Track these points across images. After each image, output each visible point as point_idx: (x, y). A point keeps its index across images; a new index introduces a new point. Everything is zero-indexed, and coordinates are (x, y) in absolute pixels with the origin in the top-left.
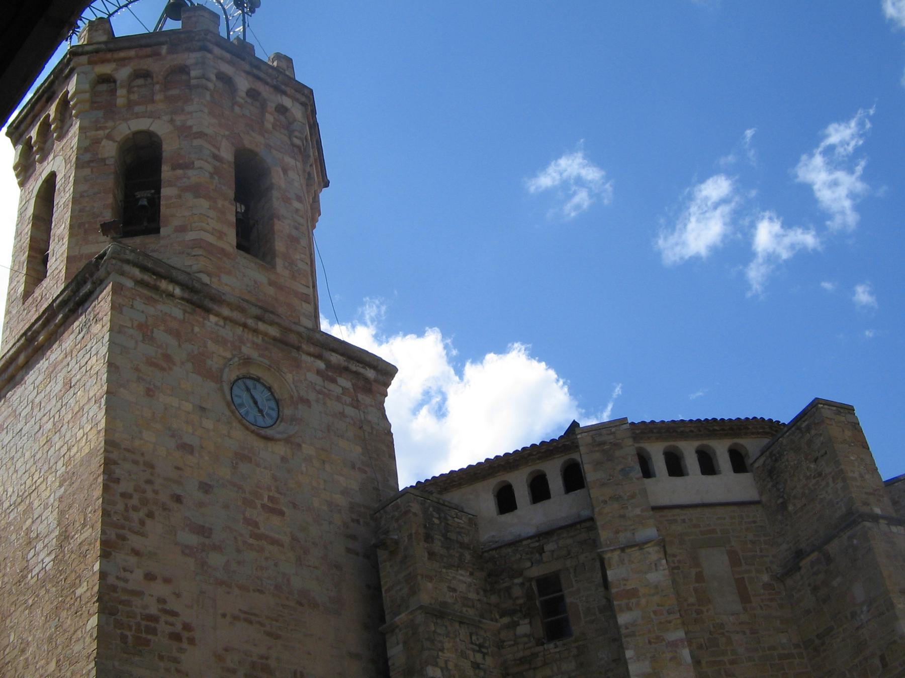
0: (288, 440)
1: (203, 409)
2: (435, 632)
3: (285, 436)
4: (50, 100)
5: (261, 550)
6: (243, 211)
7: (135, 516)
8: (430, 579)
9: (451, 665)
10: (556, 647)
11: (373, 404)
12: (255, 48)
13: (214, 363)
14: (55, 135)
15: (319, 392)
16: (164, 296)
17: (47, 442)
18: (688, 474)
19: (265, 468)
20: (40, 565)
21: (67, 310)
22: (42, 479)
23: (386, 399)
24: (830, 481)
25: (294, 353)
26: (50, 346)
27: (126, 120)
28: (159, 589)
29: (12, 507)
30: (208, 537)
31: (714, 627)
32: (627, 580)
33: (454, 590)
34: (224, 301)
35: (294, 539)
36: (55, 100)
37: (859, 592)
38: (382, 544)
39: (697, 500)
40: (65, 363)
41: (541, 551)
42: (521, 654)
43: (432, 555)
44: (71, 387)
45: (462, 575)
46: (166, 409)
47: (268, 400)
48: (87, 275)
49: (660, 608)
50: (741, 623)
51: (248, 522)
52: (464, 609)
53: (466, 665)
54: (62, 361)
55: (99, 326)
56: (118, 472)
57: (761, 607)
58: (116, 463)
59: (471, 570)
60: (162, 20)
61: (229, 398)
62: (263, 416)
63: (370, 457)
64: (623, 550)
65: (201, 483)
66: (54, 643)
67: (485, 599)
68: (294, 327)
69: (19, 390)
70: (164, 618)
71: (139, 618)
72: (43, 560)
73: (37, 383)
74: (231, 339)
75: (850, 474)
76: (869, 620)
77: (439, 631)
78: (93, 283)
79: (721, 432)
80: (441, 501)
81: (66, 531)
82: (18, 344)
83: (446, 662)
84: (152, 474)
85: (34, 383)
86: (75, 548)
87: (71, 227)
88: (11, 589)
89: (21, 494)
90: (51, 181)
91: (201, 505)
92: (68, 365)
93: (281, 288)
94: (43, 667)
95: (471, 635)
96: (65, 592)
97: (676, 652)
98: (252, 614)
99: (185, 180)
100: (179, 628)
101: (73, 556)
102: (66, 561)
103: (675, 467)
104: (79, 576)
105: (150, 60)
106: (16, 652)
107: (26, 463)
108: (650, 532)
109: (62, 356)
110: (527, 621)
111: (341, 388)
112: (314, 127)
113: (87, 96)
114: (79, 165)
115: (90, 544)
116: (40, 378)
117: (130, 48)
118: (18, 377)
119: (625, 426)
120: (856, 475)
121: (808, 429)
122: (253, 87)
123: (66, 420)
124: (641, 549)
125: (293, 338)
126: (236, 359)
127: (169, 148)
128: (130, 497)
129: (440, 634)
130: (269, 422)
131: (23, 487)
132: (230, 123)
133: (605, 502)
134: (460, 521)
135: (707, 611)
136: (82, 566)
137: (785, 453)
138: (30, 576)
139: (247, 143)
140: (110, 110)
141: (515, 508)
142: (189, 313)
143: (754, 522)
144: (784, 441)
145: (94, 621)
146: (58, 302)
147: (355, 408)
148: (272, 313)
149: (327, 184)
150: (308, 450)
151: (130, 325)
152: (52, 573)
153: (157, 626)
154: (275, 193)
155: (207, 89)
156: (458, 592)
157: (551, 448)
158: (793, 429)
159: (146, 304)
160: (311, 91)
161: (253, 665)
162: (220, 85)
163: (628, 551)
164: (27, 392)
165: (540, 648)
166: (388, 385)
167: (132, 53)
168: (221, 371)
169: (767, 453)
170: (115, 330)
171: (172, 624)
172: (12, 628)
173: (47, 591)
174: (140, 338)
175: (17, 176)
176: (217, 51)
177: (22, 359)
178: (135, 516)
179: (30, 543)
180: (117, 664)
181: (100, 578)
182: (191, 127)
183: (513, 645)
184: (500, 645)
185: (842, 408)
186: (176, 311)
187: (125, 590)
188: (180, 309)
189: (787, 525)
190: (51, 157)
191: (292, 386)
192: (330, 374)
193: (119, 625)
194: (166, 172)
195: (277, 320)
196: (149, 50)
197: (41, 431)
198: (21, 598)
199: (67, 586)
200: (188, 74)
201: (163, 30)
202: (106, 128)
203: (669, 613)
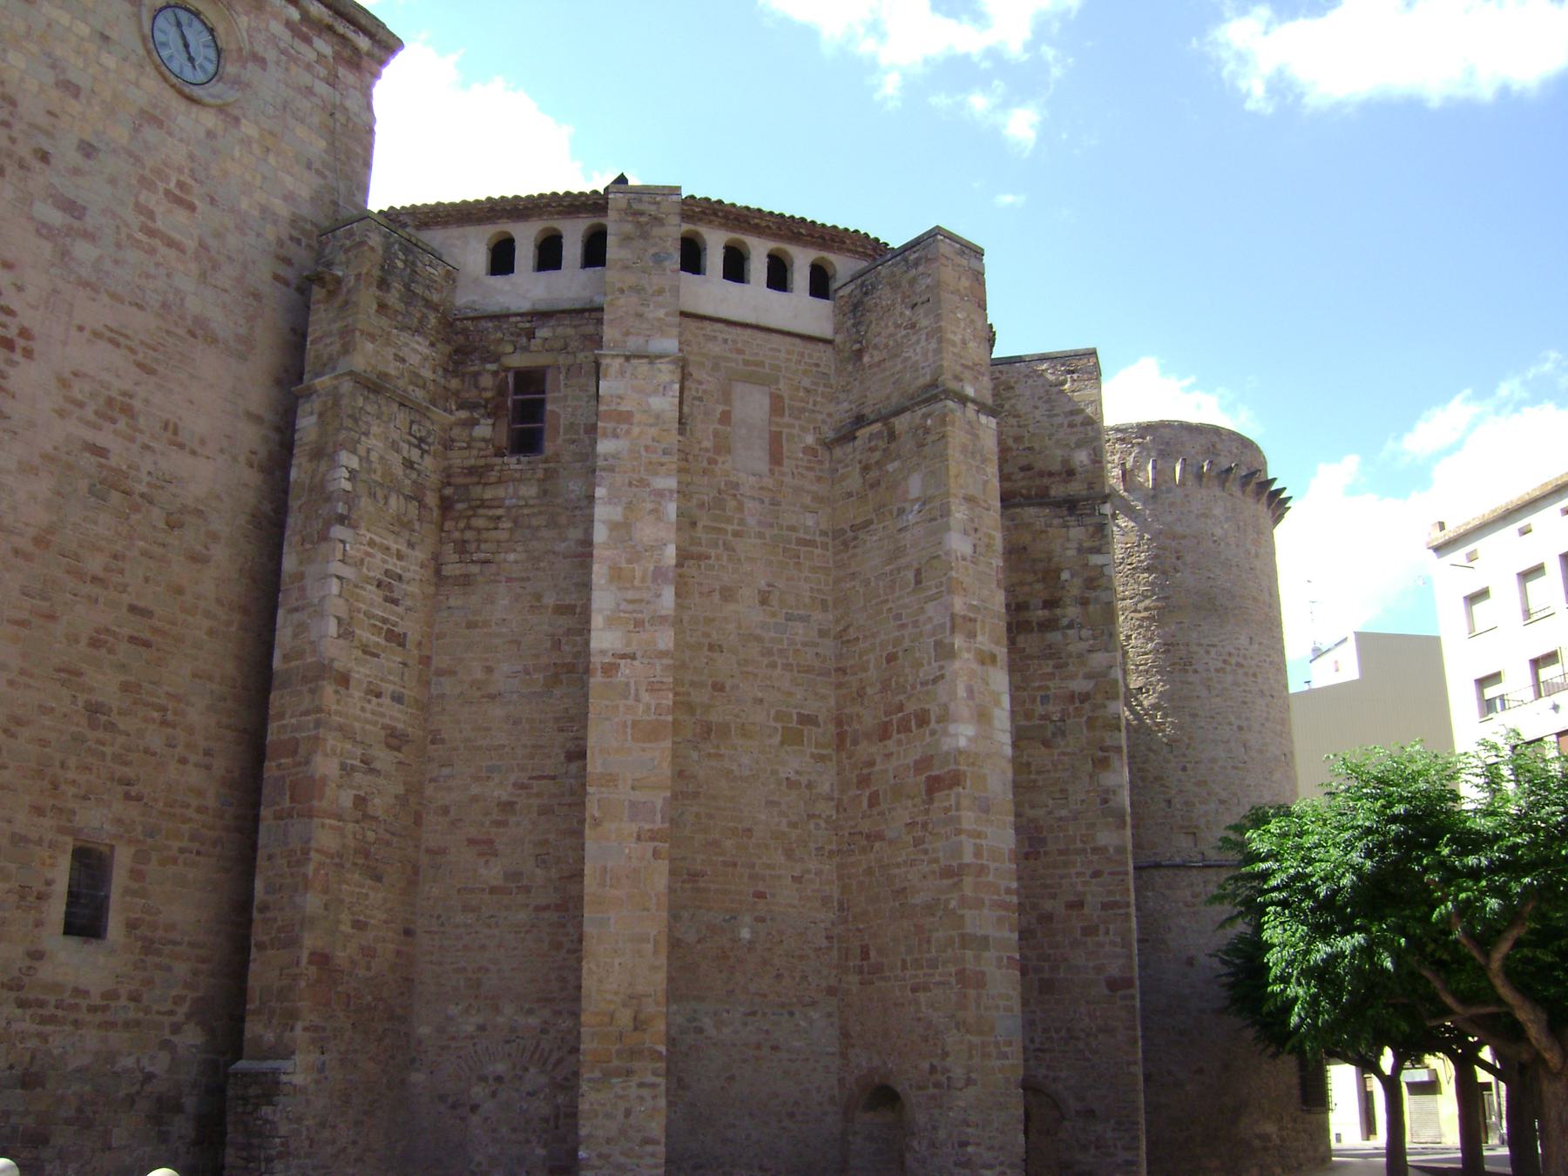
0: (221, 109)
1: (105, 38)
2: (362, 408)
3: (219, 102)
5: (152, 251)
8: (372, 337)
9: (374, 456)
10: (519, 462)
11: (359, 86)
15: (283, 52)
19: (181, 140)
24: (923, 337)
30: (79, 218)
31: (726, 484)
32: (621, 398)
33: (403, 360)
35: (203, 246)
37: (915, 486)
38: (317, 279)
41: (531, 335)
42: (472, 462)
43: (382, 307)
45: (418, 343)
46: (49, 25)
49: (656, 444)
50: (761, 488)
51: (141, 209)
52: (411, 388)
53: (395, 460)
61: (147, 30)
62: (194, 67)
64: (628, 358)
65: (82, 141)
67: (443, 381)
75: (950, 336)
76: (917, 523)
77: (369, 408)
80: (413, 240)
83: (369, 451)
84: (11, 114)
91: (76, 171)
95: (412, 422)
97: (660, 503)
103: (735, 267)
110: (490, 421)
119: (675, 198)
120: (957, 339)
121: (916, 264)
129: (369, 413)
130: (201, 77)
133: (622, 291)
134: (433, 271)
135: (723, 463)
144: (883, 270)
150: (248, 129)
158: (898, 258)
161: (110, 402)
163: (635, 362)
165: (498, 460)
166: (383, 63)
169: (859, 281)
183: (465, 449)
184: (448, 444)
185: (967, 247)
189: (855, 380)
191: (245, 34)
192: (304, 29)
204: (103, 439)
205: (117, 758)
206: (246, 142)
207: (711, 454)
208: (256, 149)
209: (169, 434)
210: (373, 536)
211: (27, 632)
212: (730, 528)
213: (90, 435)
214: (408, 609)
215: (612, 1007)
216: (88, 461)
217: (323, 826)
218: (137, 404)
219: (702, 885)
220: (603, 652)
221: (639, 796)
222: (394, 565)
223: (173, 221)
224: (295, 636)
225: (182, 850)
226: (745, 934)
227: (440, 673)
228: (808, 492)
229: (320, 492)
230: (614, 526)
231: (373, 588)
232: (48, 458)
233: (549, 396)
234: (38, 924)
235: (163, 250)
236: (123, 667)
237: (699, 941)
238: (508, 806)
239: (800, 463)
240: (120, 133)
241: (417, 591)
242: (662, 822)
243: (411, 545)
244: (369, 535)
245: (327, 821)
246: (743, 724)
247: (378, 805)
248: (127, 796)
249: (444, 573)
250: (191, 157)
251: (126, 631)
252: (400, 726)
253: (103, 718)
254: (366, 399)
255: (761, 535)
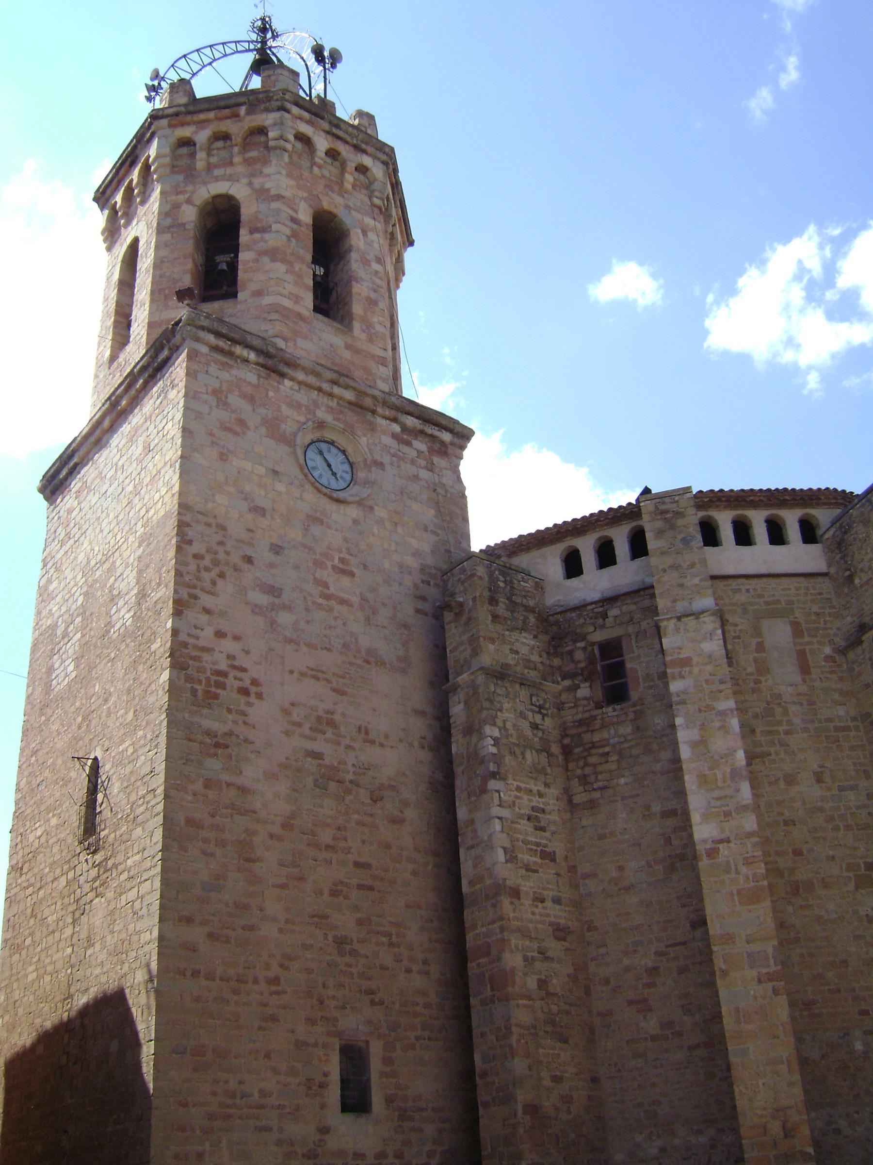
0: (359, 503)
1: (276, 473)
2: (494, 692)
3: (357, 499)
4: (133, 164)
5: (330, 610)
6: (322, 274)
7: (206, 576)
8: (492, 640)
9: (509, 725)
10: (614, 710)
12: (336, 106)
13: (288, 428)
14: (138, 200)
16: (239, 361)
17: (129, 503)
18: (755, 544)
19: (337, 530)
20: (121, 621)
21: (147, 375)
22: (123, 539)
23: (462, 462)
25: (369, 416)
26: (132, 411)
27: (205, 183)
28: (228, 645)
29: (98, 565)
30: (278, 597)
32: (680, 649)
33: (517, 652)
34: (299, 365)
35: (364, 599)
36: (138, 164)
38: (446, 606)
39: (763, 570)
40: (145, 428)
41: (605, 616)
42: (580, 716)
43: (495, 617)
44: (150, 451)
46: (239, 472)
47: (342, 463)
48: (164, 342)
50: (799, 694)
51: (318, 582)
52: (526, 671)
53: (525, 725)
54: (142, 425)
55: (175, 392)
56: (191, 533)
57: (820, 678)
58: (188, 525)
59: (535, 633)
60: (248, 77)
61: (302, 461)
63: (443, 520)
64: (679, 618)
65: (272, 544)
66: (132, 694)
67: (548, 662)
68: (370, 391)
69: (105, 453)
70: (233, 673)
71: (208, 674)
72: (123, 616)
73: (121, 446)
74: (306, 403)
77: (499, 691)
78: (170, 349)
79: (792, 502)
80: (508, 565)
81: (143, 590)
82: (104, 408)
83: (504, 722)
85: (117, 446)
86: (150, 607)
87: (153, 292)
88: (96, 643)
89: (105, 553)
90: (134, 245)
91: (272, 565)
92: (148, 429)
93: (357, 351)
94: (122, 716)
95: (531, 696)
96: (142, 647)
97: (725, 720)
98: (319, 671)
99: (262, 244)
100: (247, 683)
101: (150, 614)
102: (143, 618)
104: (154, 633)
105: (229, 121)
106: (100, 701)
107: (110, 523)
108: (708, 602)
109: (142, 420)
110: (587, 684)
111: (416, 452)
112: (396, 186)
113: (167, 160)
114: (161, 230)
115: (164, 603)
116: (123, 442)
117: (208, 110)
118: (104, 440)
122: (333, 146)
123: (145, 483)
124: (697, 618)
125: (368, 402)
126: (310, 423)
127: (247, 212)
128: (202, 557)
130: (343, 485)
131: (107, 546)
132: (309, 184)
133: (664, 571)
135: (766, 681)
136: (157, 623)
137: (855, 525)
138: (112, 631)
139: (326, 205)
140: (190, 174)
141: (582, 574)
142: (264, 378)
143: (821, 594)
145: (166, 676)
146: (138, 367)
147: (429, 470)
148: (347, 377)
149: (411, 243)
150: (380, 512)
151: (204, 391)
152: (131, 628)
153: (226, 680)
154: (354, 256)
155: (285, 150)
156: (521, 655)
157: (619, 514)
159: (220, 370)
160: (392, 150)
161: (319, 719)
162: (299, 145)
164: (111, 455)
165: (599, 711)
166: (463, 448)
167: (211, 115)
168: (295, 435)
169: (838, 525)
170: (190, 395)
171: (241, 680)
172: (97, 678)
173: (127, 646)
174: (214, 403)
175: (105, 241)
176: (295, 110)
177: (107, 423)
178: (206, 576)
179: (113, 600)
180: (187, 715)
181: (172, 635)
182: (268, 190)
184: (560, 707)
186: (250, 376)
187: (196, 647)
188: (254, 374)
189: (852, 598)
190: (135, 222)
191: (366, 449)
192: (405, 437)
193: (189, 679)
194: (244, 236)
195: (352, 383)
196: (227, 112)
197: (123, 493)
198: (105, 651)
199: (144, 641)
200: (266, 135)
201: (249, 88)
202: (185, 192)
203: (721, 682)
204: (319, 746)
205: (362, 975)
206: (380, 522)
207: (755, 677)
208: (388, 524)
209: (363, 734)
210: (518, 783)
211: (286, 892)
212: (781, 729)
213: (308, 745)
214: (553, 833)
215: (764, 1120)
216: (310, 764)
217: (518, 1006)
218: (337, 718)
219: (816, 1011)
220: (705, 841)
221: (754, 948)
222: (536, 802)
223: (340, 586)
224: (475, 866)
225: (417, 1038)
226: (859, 1046)
227: (585, 876)
228: (835, 690)
229: (475, 758)
230: (694, 745)
231: (525, 822)
232: (284, 766)
233: (627, 657)
234: (323, 1106)
235: (338, 607)
236: (356, 908)
237: (823, 1057)
238: (653, 971)
239: (825, 670)
240: (295, 534)
241: (557, 818)
242: (776, 965)
243: (547, 785)
244: (515, 783)
245: (521, 1002)
246: (823, 879)
247: (556, 984)
248: (373, 1003)
249: (575, 802)
250: (346, 540)
251: (354, 881)
252: (562, 921)
253: (348, 947)
254: (496, 685)
255: (806, 730)
